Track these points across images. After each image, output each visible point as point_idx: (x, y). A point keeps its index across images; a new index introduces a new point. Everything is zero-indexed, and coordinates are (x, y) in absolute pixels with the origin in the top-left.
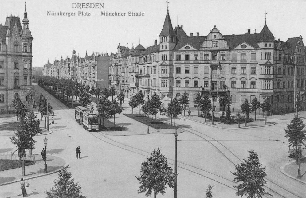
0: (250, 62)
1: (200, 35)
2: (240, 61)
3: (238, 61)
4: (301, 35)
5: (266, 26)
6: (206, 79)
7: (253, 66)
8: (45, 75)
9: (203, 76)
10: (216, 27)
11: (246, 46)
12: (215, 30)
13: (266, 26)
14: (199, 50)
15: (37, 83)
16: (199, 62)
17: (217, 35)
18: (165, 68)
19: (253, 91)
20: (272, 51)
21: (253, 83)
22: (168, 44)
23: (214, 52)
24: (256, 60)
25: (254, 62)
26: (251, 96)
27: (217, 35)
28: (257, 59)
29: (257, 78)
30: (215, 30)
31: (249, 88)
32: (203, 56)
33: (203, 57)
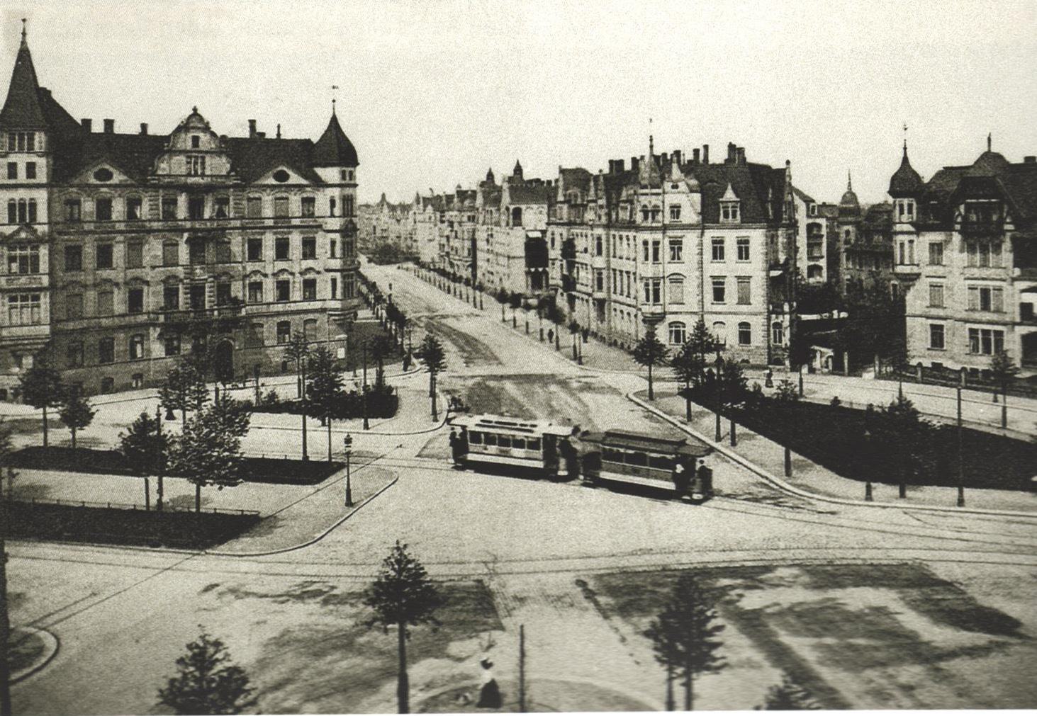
0: (301, 222)
1: (150, 132)
2: (272, 221)
3: (266, 221)
4: (706, 147)
5: (334, 120)
6: (224, 278)
7: (251, 235)
8: (786, 344)
9: (160, 273)
10: (198, 112)
11: (110, 176)
12: (194, 121)
13: (334, 120)
14: (145, 185)
15: (964, 428)
16: (144, 226)
17: (204, 137)
18: (28, 252)
19: (310, 308)
20: (41, 196)
21: (310, 286)
22: (41, 162)
23: (197, 197)
24: (287, 217)
25: (310, 222)
26: (715, 323)
27: (204, 137)
28: (320, 215)
29: (321, 269)
30: (194, 121)
31: (298, 299)
32: (157, 205)
33: (158, 209)
